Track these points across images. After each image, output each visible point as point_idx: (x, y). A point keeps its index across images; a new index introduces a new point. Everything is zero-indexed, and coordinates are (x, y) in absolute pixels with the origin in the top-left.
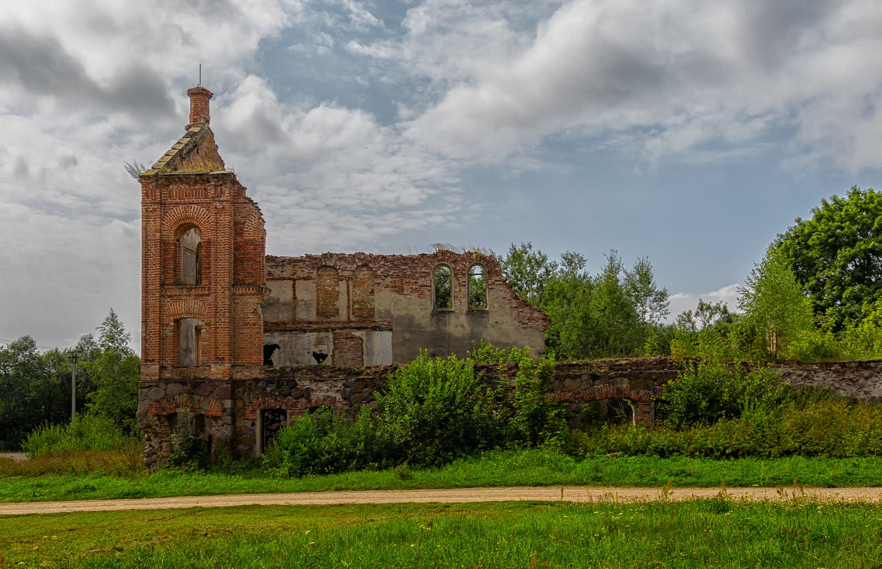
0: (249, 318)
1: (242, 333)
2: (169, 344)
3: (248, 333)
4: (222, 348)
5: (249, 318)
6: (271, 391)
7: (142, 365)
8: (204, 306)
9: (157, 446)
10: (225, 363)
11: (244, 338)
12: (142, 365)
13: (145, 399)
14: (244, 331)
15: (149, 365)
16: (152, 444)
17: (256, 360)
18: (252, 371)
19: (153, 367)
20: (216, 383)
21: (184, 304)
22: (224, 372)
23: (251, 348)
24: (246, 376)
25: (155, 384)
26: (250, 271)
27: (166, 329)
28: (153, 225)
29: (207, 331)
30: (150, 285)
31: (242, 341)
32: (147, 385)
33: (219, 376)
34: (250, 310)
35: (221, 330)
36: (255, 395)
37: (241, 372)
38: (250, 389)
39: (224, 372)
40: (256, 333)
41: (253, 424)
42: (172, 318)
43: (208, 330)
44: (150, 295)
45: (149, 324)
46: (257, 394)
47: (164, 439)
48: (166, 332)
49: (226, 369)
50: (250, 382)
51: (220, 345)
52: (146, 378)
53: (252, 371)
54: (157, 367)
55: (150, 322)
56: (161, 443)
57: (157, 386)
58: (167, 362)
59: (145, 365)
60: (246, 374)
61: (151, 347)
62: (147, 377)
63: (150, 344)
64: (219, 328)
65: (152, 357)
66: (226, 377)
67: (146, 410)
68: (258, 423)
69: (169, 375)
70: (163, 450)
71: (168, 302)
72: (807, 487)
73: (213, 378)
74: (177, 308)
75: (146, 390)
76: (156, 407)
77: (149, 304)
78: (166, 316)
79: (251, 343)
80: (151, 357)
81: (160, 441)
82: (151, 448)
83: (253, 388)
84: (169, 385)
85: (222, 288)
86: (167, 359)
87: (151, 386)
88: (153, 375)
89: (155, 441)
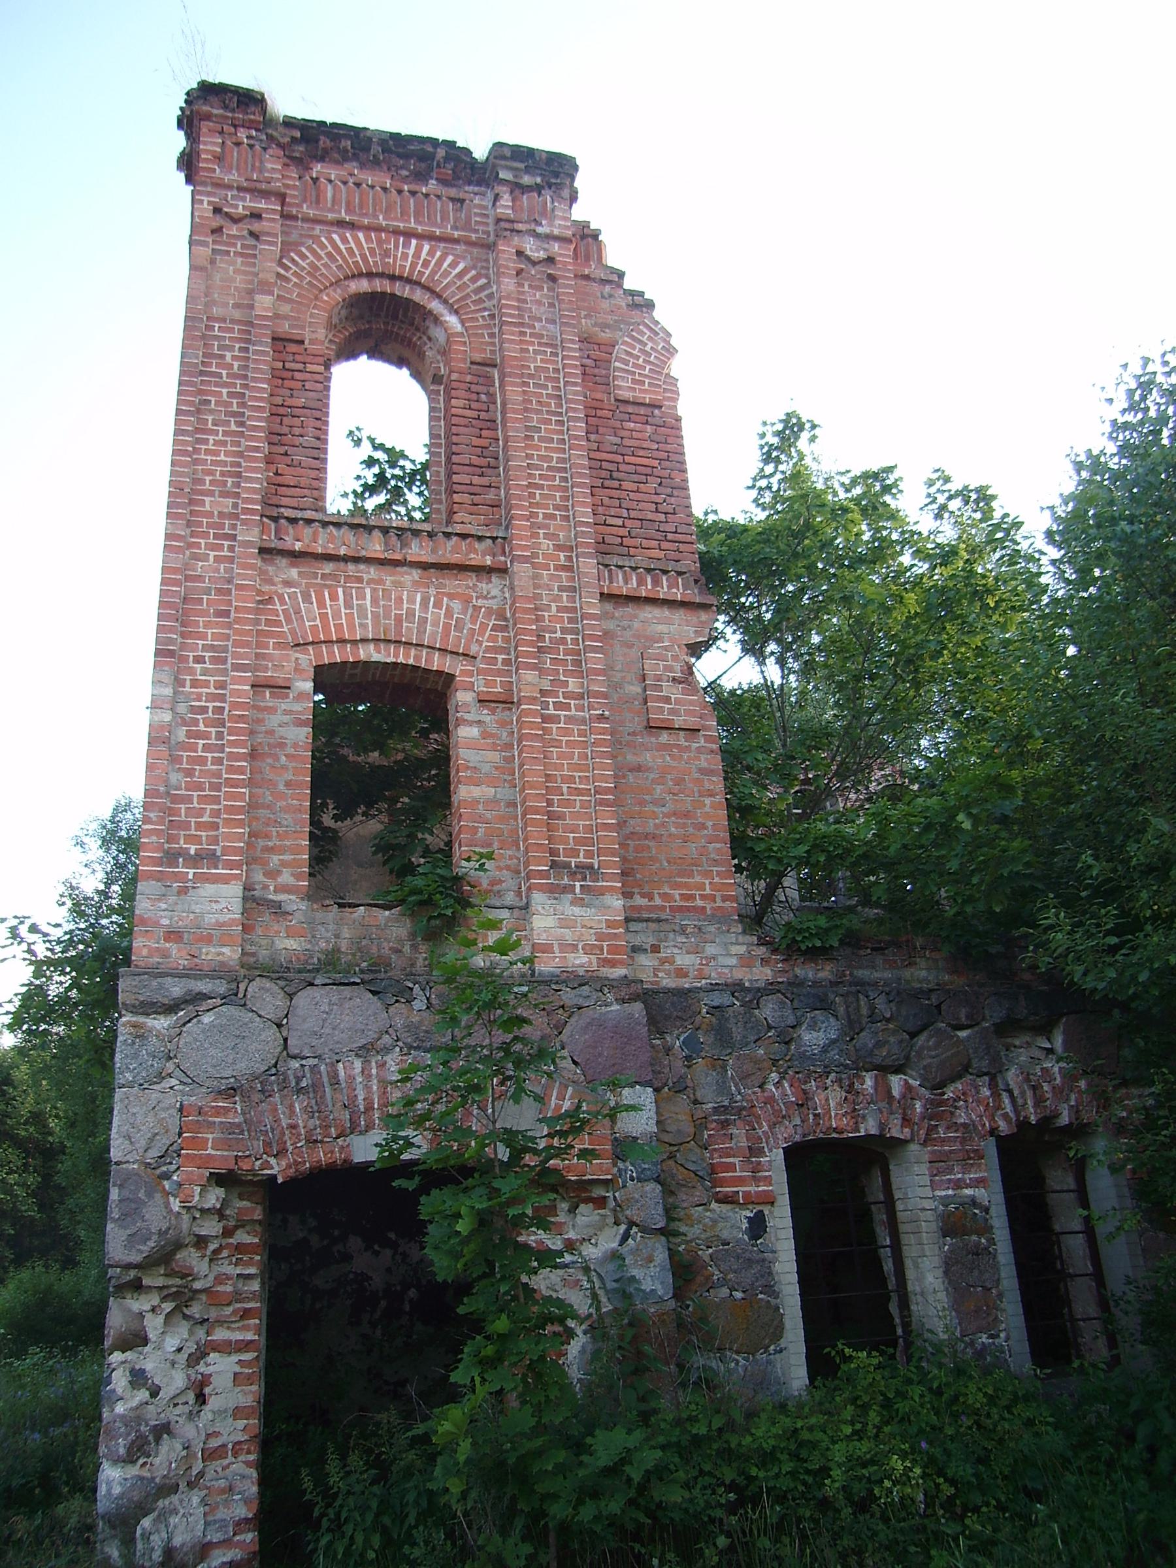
0: (667, 700)
1: (639, 768)
2: (288, 784)
3: (664, 771)
4: (576, 816)
5: (667, 700)
6: (825, 1049)
7: (150, 876)
8: (474, 619)
9: (178, 1380)
10: (602, 892)
11: (650, 792)
12: (150, 876)
13: (161, 1077)
14: (648, 758)
15: (182, 877)
16: (149, 1366)
17: (713, 898)
18: (710, 950)
19: (209, 889)
20: (568, 996)
21: (375, 601)
22: (600, 937)
23: (686, 839)
24: (681, 973)
25: (222, 987)
26: (650, 516)
27: (272, 710)
28: (232, 270)
29: (485, 735)
30: (211, 493)
31: (642, 803)
32: (176, 989)
33: (580, 961)
34: (669, 668)
35: (566, 732)
36: (748, 1067)
37: (656, 949)
38: (723, 1036)
39: (600, 937)
40: (703, 771)
41: (758, 1226)
42: (307, 659)
43: (493, 728)
44: (205, 535)
45: (191, 671)
46: (756, 1061)
47: (220, 1334)
48: (273, 721)
49: (610, 924)
50: (717, 999)
51: (568, 803)
52: (165, 954)
53: (710, 950)
54: (232, 893)
55: (199, 660)
56: (195, 1359)
57: (232, 998)
58: (272, 874)
59: (159, 877)
60: (684, 960)
61: (199, 787)
62: (173, 948)
63: (189, 773)
64: (554, 719)
65: (196, 840)
66: (612, 964)
67: (162, 1143)
68: (781, 1219)
69: (292, 944)
70: (214, 1403)
71: (288, 583)
72: (1062, 1264)
73: (546, 965)
74: (336, 615)
75: (160, 1023)
76: (230, 1128)
77: (200, 578)
78: (278, 646)
79: (687, 815)
80: (190, 839)
81: (191, 1348)
82: (143, 1395)
83: (737, 1032)
84: (304, 999)
85: (559, 548)
86: (275, 859)
87: (203, 997)
88: (209, 940)
89: (171, 1343)
